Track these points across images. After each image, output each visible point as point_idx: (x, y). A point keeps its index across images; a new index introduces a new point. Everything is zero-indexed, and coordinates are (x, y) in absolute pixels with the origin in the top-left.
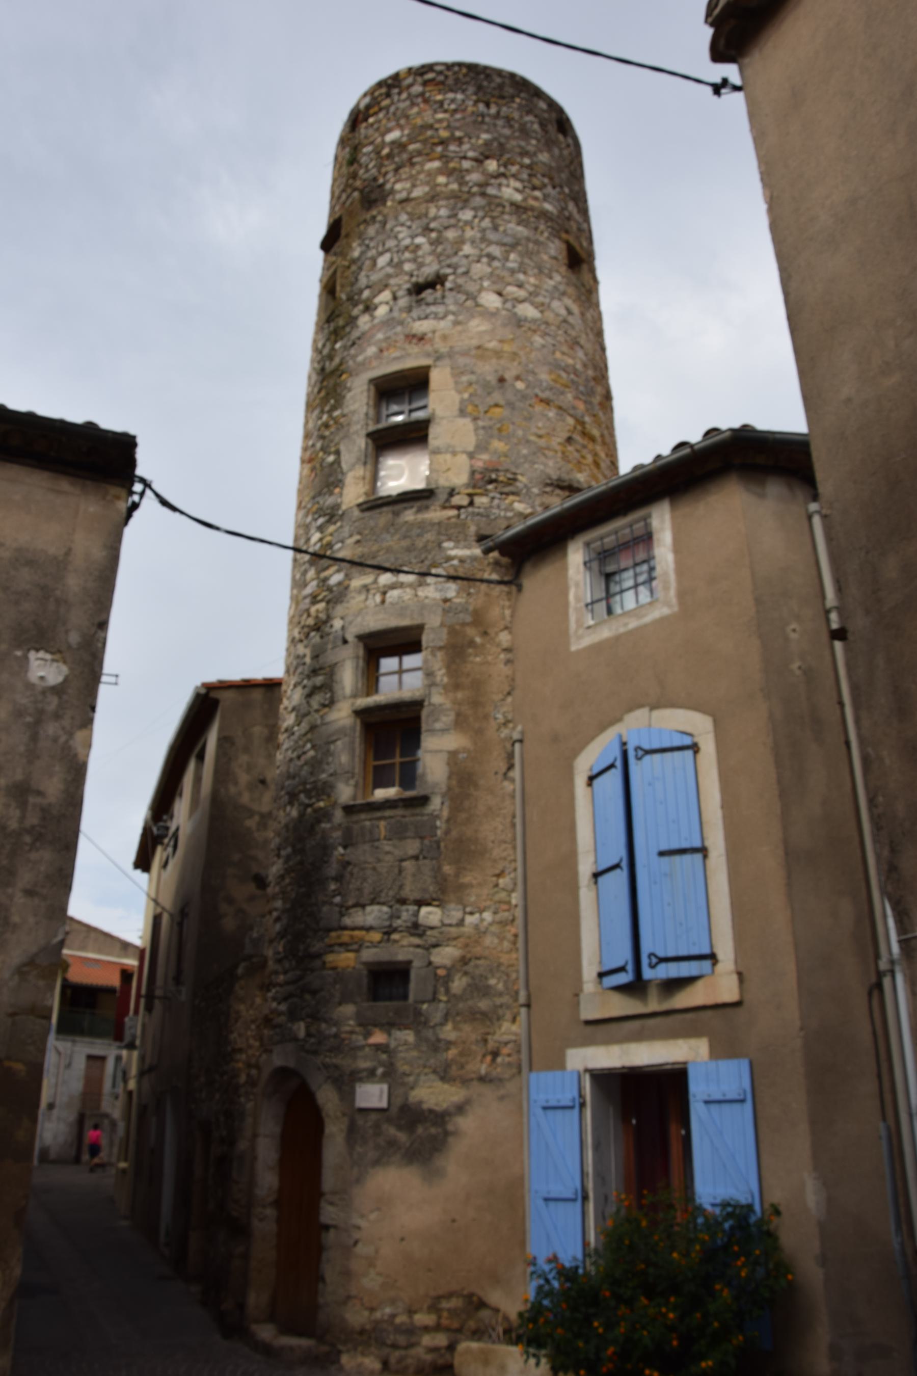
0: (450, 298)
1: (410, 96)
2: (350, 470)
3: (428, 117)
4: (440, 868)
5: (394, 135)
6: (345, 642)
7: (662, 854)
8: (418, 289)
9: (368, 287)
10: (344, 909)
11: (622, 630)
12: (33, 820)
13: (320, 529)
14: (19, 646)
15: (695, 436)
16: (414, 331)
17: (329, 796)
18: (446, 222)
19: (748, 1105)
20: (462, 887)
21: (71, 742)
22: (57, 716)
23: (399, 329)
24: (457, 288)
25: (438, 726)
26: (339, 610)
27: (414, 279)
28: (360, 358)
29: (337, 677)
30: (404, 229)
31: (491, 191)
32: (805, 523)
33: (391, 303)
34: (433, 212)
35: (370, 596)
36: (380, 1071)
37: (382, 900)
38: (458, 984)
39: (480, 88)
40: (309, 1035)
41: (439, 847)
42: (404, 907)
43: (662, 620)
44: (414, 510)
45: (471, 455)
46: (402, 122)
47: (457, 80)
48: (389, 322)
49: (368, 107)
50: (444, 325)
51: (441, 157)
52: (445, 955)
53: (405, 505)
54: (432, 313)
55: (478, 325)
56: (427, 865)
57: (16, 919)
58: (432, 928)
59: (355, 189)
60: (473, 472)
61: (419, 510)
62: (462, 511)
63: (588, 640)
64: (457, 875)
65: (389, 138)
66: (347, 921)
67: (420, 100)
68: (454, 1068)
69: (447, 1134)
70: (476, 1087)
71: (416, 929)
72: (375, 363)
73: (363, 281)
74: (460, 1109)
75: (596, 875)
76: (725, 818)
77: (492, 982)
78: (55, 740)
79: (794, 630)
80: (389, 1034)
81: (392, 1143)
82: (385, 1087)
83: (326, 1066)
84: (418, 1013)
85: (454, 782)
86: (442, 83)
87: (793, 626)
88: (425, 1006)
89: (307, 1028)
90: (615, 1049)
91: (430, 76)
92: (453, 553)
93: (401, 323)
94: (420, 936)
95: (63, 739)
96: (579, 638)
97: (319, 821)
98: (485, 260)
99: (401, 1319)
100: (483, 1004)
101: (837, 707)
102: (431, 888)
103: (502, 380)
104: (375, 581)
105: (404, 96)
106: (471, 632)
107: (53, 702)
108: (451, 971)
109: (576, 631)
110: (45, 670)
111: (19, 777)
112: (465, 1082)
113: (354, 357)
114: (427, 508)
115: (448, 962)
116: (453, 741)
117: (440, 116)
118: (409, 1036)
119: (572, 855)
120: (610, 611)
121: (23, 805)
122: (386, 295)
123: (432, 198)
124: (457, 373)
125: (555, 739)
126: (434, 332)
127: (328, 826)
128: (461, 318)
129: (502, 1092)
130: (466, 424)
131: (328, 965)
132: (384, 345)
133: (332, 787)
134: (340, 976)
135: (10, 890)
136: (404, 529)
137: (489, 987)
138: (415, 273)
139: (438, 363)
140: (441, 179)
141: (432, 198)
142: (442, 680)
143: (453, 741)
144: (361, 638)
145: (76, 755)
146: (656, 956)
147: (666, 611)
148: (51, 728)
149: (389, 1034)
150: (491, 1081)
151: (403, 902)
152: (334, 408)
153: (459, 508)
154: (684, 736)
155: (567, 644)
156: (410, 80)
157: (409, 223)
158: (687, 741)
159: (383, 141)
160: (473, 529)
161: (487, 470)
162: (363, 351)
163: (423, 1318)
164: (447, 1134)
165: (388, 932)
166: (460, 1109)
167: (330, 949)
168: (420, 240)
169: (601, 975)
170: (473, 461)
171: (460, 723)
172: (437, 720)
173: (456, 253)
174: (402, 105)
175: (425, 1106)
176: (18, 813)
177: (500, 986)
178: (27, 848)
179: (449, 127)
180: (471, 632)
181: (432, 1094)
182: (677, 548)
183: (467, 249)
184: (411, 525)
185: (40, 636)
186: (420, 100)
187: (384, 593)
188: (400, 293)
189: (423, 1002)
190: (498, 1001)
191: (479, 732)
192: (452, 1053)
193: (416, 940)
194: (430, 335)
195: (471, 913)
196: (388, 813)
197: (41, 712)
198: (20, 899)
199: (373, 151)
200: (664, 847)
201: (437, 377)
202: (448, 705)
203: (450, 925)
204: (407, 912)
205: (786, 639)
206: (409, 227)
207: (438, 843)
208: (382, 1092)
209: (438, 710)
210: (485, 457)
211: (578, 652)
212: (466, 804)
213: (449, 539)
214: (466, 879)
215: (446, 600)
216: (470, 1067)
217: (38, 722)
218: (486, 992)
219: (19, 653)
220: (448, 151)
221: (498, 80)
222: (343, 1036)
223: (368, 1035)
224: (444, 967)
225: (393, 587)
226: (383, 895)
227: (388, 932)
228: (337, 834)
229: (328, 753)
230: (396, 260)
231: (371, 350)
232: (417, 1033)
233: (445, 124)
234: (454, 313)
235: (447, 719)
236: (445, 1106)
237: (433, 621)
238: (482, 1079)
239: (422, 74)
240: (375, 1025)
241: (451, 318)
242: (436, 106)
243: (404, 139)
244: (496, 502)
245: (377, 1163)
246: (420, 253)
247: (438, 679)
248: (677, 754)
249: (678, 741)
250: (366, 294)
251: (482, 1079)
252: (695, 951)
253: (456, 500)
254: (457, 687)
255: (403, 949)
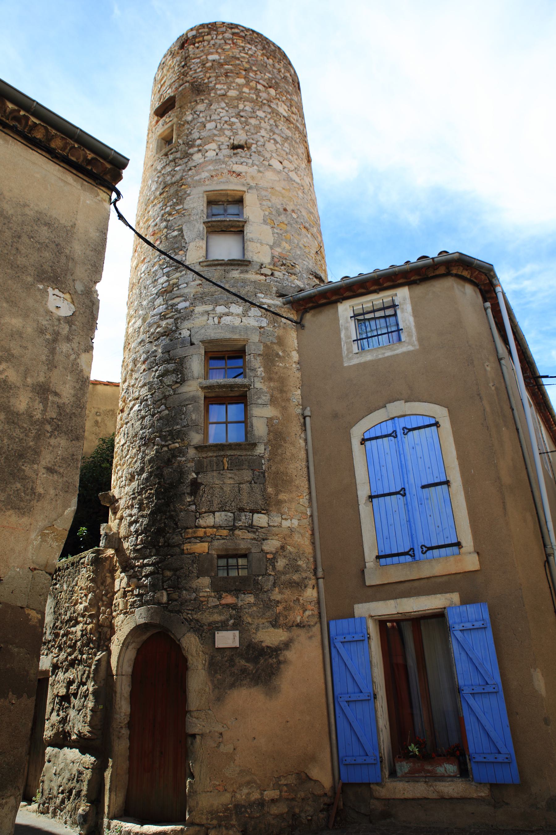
0: (255, 157)
1: (223, 38)
2: (192, 241)
3: (236, 52)
4: (265, 489)
5: (215, 57)
6: (192, 344)
7: (423, 487)
8: (234, 147)
9: (199, 138)
10: (198, 514)
11: (380, 356)
12: (52, 413)
13: (168, 275)
14: (41, 281)
15: (433, 253)
16: (234, 170)
17: (183, 440)
18: (250, 115)
19: (489, 633)
20: (279, 503)
21: (78, 360)
22: (68, 339)
23: (224, 166)
24: (259, 153)
25: (260, 401)
26: (187, 324)
27: (232, 141)
28: (197, 178)
29: (187, 365)
30: (224, 111)
31: (273, 105)
32: (484, 312)
33: (217, 151)
34: (241, 106)
35: (211, 318)
36: (231, 622)
37: (227, 508)
38: (281, 563)
39: (264, 48)
40: (169, 599)
41: (264, 477)
42: (243, 514)
43: (408, 353)
44: (239, 271)
45: (272, 248)
46: (219, 51)
47: (252, 39)
48: (216, 161)
49: (194, 37)
50: (253, 170)
51: (245, 78)
52: (271, 545)
53: (232, 267)
54: (244, 162)
55: (269, 175)
56: (257, 488)
57: (40, 490)
58: (262, 528)
59: (187, 82)
60: (273, 257)
61: (242, 272)
62: (267, 277)
63: (355, 361)
64: (277, 494)
65: (211, 57)
66: (201, 522)
67: (230, 42)
68: (281, 618)
69: (279, 662)
70: (296, 631)
71: (251, 528)
72: (207, 182)
73: (195, 135)
74: (287, 645)
75: (371, 497)
76: (460, 464)
77: (300, 563)
78: (68, 356)
79: (487, 366)
80: (238, 598)
81: (244, 671)
82: (237, 633)
83: (190, 621)
84: (257, 583)
85: (271, 437)
86: (244, 37)
87: (486, 364)
88: (260, 578)
89: (168, 595)
90: (392, 603)
91: (236, 31)
92: (264, 301)
93: (224, 162)
94: (254, 532)
95: (73, 357)
96: (350, 359)
97: (174, 456)
98: (272, 141)
99: (256, 796)
100: (296, 577)
101: (510, 410)
102: (260, 502)
103: (285, 210)
104: (214, 310)
105: (220, 37)
106: (276, 347)
107: (65, 329)
108: (275, 555)
109: (347, 355)
110: (60, 304)
111: (42, 379)
112: (289, 627)
113: (192, 177)
114: (247, 272)
115: (274, 550)
116: (269, 412)
117: (243, 55)
118: (251, 599)
119: (351, 486)
120: (399, 339)
121: (44, 401)
122: (213, 146)
123: (240, 98)
124: (261, 199)
125: (335, 416)
126: (246, 173)
127: (184, 459)
128: (261, 169)
129: (311, 634)
130: (267, 229)
131: (186, 551)
132: (214, 173)
133: (185, 434)
134: (196, 558)
135: (35, 466)
136: (232, 281)
137: (299, 566)
138: (232, 138)
139: (249, 191)
140: (246, 90)
141: (240, 98)
142: (261, 374)
143: (269, 412)
144: (207, 343)
145: (82, 371)
146: (426, 547)
147: (411, 348)
148: (64, 347)
149: (238, 598)
150: (304, 626)
151: (242, 510)
152: (177, 204)
153: (266, 275)
154: (431, 418)
155: (342, 362)
156: (224, 29)
157: (227, 109)
158: (433, 421)
159: (207, 59)
160: (275, 289)
161: (281, 257)
162: (198, 173)
163: (270, 794)
164: (279, 662)
165: (233, 529)
166: (287, 645)
167: (189, 540)
168: (233, 120)
169: (378, 557)
170: (273, 251)
171: (273, 401)
172: (259, 398)
173: (256, 133)
174: (218, 42)
175: (264, 645)
176: (41, 406)
177: (304, 565)
178: (49, 435)
179: (248, 62)
180: (276, 347)
181: (271, 637)
182: (415, 313)
183: (263, 133)
184: (237, 280)
185: (56, 278)
186: (230, 42)
187: (220, 318)
188: (223, 147)
189: (259, 576)
190: (304, 575)
191: (284, 408)
192: (280, 608)
193: (251, 535)
194: (244, 174)
195: (286, 519)
196: (229, 453)
197: (57, 333)
198: (43, 475)
199: (200, 62)
200: (424, 483)
201: (249, 199)
202: (265, 389)
203: (274, 526)
204: (244, 519)
205: (485, 370)
206: (227, 111)
207: (263, 473)
208: (234, 636)
209: (259, 392)
210: (279, 250)
211: (350, 367)
212: (280, 451)
213: (262, 293)
214: (282, 496)
215: (261, 328)
216: (291, 617)
217: (55, 340)
218: (297, 569)
219: (41, 287)
220: (249, 75)
221: (273, 47)
222: (201, 599)
223: (220, 598)
224: (271, 553)
225: (227, 314)
226: (228, 505)
227: (233, 529)
228: (191, 465)
229: (181, 413)
230: (219, 126)
231: (204, 175)
232: (256, 596)
233: (246, 60)
234: (257, 165)
235: (265, 398)
236: (276, 643)
237: (255, 338)
238: (299, 626)
239: (232, 28)
240: (226, 592)
241: (255, 167)
242: (241, 49)
243: (222, 61)
244: (286, 277)
245: (232, 686)
246: (234, 127)
247: (259, 373)
248: (427, 429)
249: (427, 421)
250: (198, 142)
251: (299, 626)
252: (448, 542)
253: (263, 271)
254: (270, 379)
255: (244, 539)
